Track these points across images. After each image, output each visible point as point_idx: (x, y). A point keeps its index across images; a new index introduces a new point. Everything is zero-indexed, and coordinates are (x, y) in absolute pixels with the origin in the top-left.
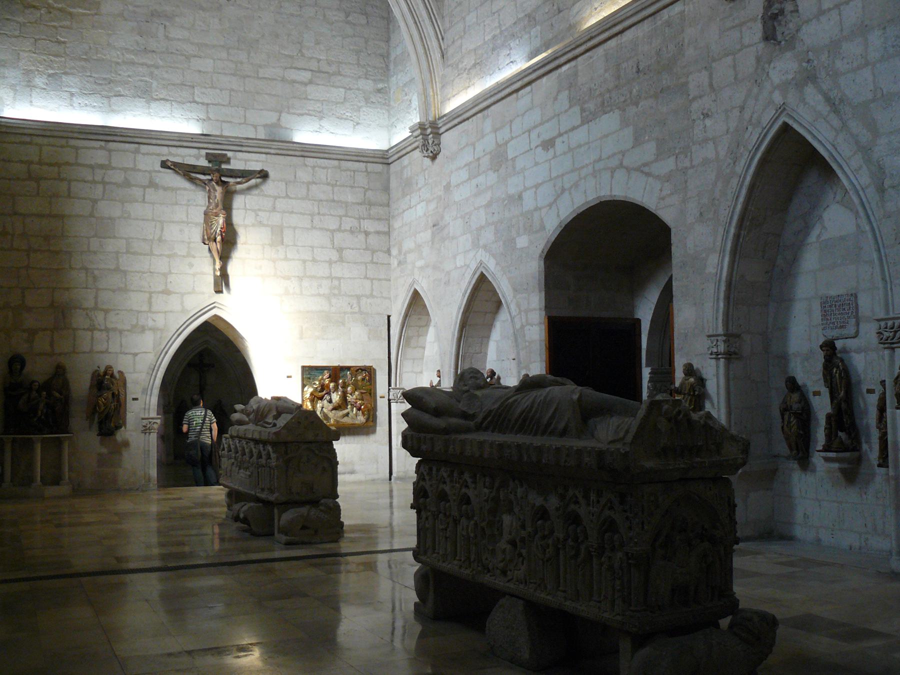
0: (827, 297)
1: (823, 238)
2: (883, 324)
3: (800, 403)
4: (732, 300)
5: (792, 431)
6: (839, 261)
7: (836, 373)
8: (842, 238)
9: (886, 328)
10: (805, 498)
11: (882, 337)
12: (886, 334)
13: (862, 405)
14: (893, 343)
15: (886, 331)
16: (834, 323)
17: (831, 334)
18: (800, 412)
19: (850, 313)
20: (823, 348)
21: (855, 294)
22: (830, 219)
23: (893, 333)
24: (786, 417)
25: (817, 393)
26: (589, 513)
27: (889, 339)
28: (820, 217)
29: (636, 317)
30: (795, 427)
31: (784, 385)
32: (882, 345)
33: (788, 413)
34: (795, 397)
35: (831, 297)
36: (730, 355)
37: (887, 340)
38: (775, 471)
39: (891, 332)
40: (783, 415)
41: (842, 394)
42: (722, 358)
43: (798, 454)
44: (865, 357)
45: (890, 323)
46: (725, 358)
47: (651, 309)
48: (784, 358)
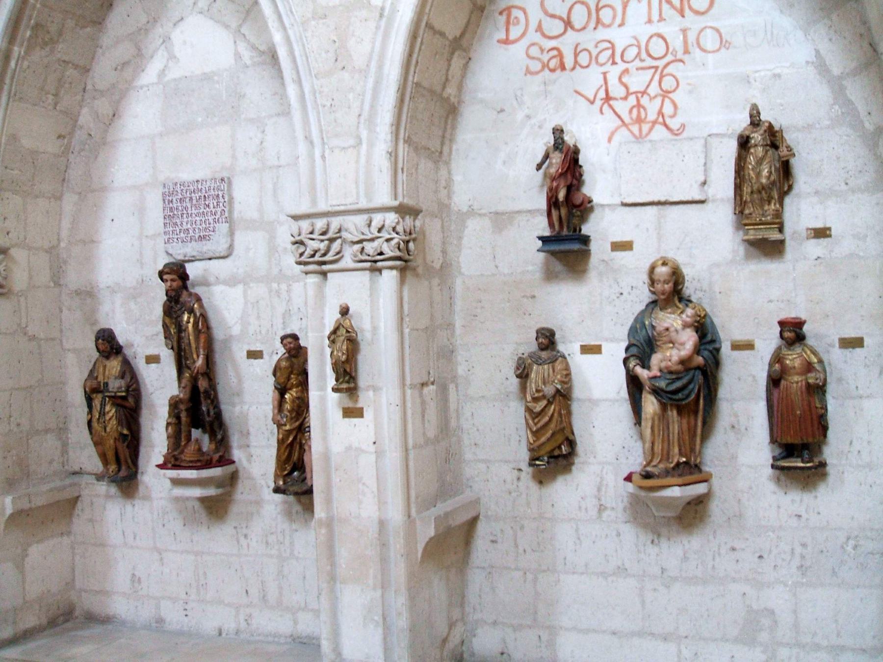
0: (176, 184)
1: (166, 79)
2: (305, 225)
3: (123, 377)
5: (108, 429)
6: (200, 119)
7: (188, 322)
8: (207, 77)
9: (311, 233)
10: (132, 547)
11: (302, 249)
12: (313, 245)
13: (234, 380)
14: (324, 263)
15: (313, 239)
17: (179, 252)
18: (124, 394)
19: (219, 213)
20: (165, 277)
21: (229, 178)
22: (185, 42)
23: (326, 242)
24: (97, 403)
25: (152, 359)
27: (318, 255)
28: (166, 40)
30: (114, 422)
31: (92, 345)
33: (100, 396)
34: (114, 365)
37: (313, 256)
38: (75, 501)
39: (322, 241)
40: (89, 401)
41: (200, 362)
43: (119, 470)
44: (245, 292)
45: (320, 224)
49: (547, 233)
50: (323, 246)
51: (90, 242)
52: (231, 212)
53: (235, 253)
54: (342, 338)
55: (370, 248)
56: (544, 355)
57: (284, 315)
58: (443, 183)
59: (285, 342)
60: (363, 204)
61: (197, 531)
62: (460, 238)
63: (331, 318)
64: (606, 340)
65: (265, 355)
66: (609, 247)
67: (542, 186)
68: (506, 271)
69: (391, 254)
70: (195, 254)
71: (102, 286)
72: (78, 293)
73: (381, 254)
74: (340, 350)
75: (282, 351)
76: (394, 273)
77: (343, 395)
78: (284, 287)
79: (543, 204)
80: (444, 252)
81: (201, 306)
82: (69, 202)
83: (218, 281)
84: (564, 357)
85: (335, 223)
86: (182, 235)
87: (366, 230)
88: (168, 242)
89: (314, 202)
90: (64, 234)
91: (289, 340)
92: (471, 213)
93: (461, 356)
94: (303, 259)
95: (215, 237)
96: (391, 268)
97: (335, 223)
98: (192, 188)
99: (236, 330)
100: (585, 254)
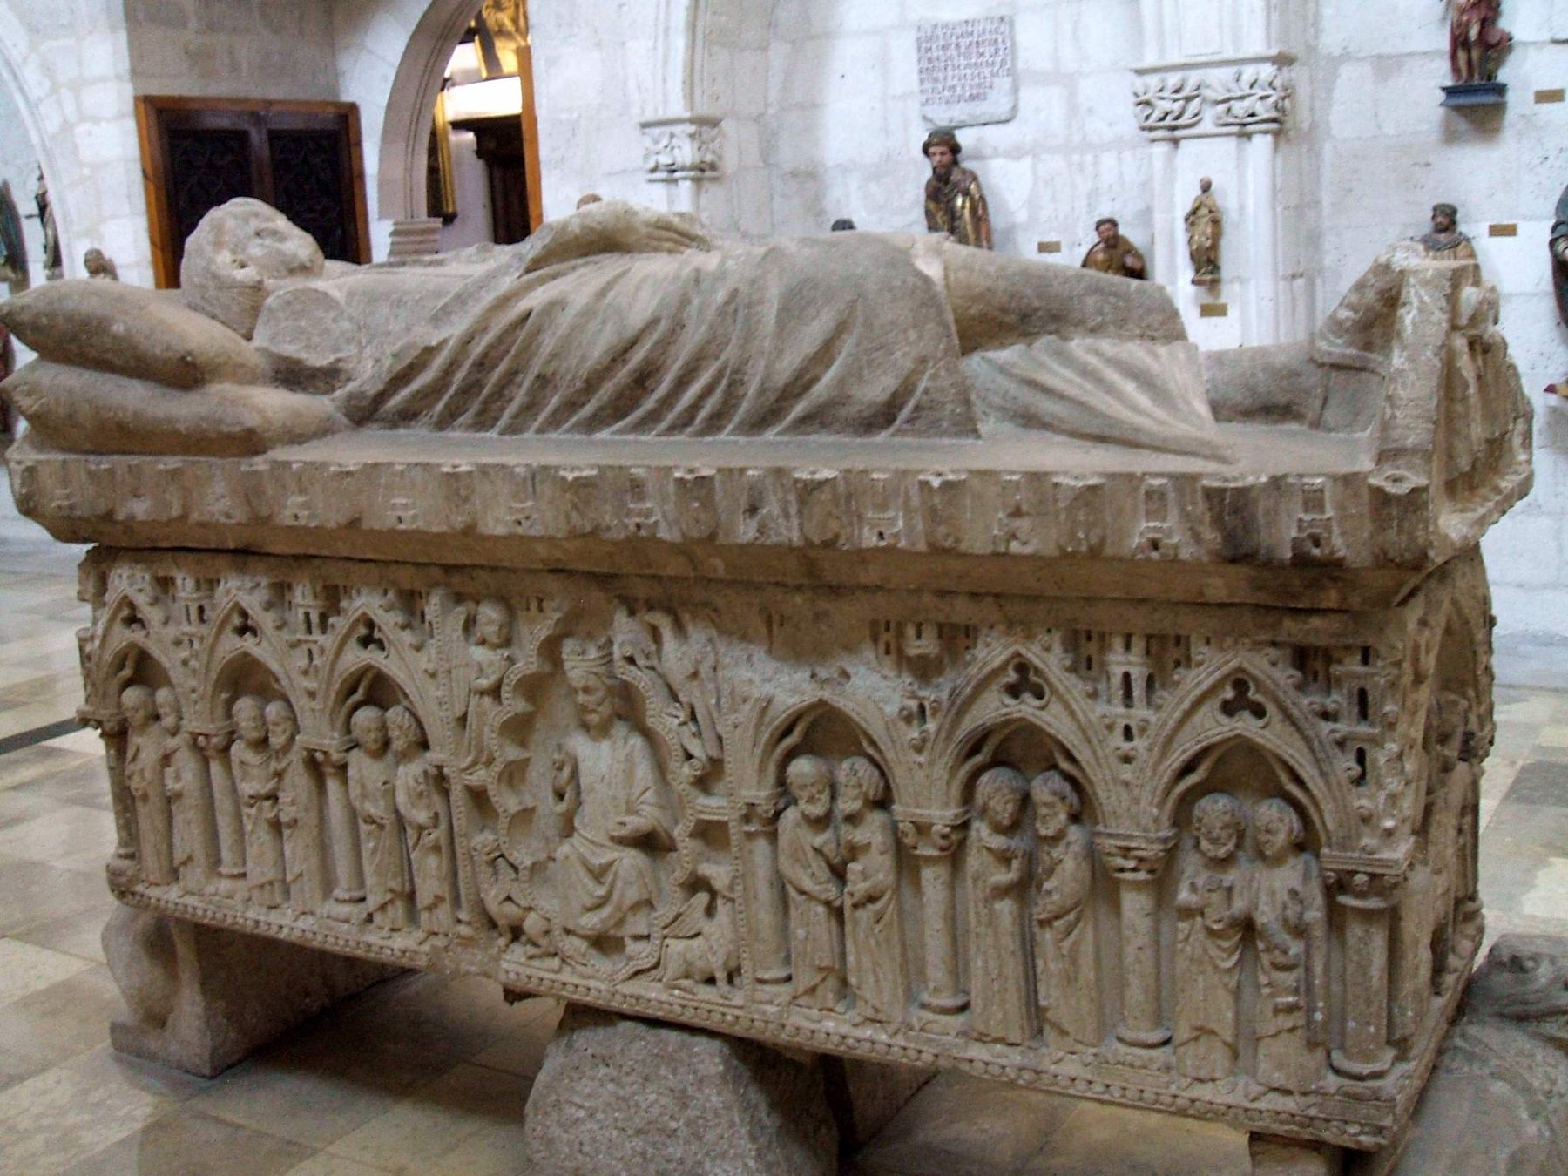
0: (935, 26)
2: (1153, 81)
4: (700, 36)
7: (963, 207)
14: (1174, 128)
16: (953, 88)
17: (943, 116)
26: (1110, 727)
27: (1169, 118)
29: (346, 98)
32: (1146, 134)
35: (946, 26)
36: (702, 170)
37: (1163, 119)
39: (1175, 101)
42: (685, 179)
44: (1034, 166)
45: (1173, 79)
46: (692, 179)
47: (385, 77)
48: (809, 177)
49: (1449, 83)
50: (1177, 107)
51: (811, 106)
52: (1013, 60)
53: (1020, 115)
54: (1204, 220)
55: (1239, 108)
56: (1443, 237)
57: (1089, 196)
58: (1311, 19)
59: (1102, 228)
60: (1229, 54)
61: (1254, 375)
62: (1330, 91)
63: (1186, 196)
64: (1524, 218)
65: (1064, 248)
66: (1531, 98)
67: (1444, 19)
68: (1392, 132)
69: (1266, 115)
70: (964, 117)
71: (829, 164)
72: (794, 174)
73: (1252, 115)
74: (1203, 233)
75: (1094, 238)
76: (1269, 138)
77: (1202, 289)
78: (1089, 158)
79: (1444, 43)
80: (1312, 109)
81: (979, 186)
82: (778, 53)
83: (996, 153)
84: (1468, 240)
85: (1193, 78)
86: (946, 93)
87: (1233, 86)
88: (927, 102)
89: (1162, 51)
90: (773, 96)
91: (1107, 226)
92: (1346, 57)
93: (1329, 242)
94: (1150, 122)
95: (992, 95)
96: (1266, 132)
97: (1193, 78)
98: (959, 31)
99: (1021, 216)
100: (1499, 109)
